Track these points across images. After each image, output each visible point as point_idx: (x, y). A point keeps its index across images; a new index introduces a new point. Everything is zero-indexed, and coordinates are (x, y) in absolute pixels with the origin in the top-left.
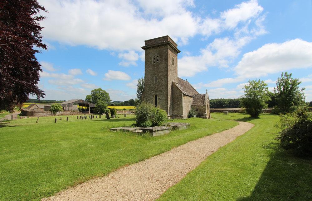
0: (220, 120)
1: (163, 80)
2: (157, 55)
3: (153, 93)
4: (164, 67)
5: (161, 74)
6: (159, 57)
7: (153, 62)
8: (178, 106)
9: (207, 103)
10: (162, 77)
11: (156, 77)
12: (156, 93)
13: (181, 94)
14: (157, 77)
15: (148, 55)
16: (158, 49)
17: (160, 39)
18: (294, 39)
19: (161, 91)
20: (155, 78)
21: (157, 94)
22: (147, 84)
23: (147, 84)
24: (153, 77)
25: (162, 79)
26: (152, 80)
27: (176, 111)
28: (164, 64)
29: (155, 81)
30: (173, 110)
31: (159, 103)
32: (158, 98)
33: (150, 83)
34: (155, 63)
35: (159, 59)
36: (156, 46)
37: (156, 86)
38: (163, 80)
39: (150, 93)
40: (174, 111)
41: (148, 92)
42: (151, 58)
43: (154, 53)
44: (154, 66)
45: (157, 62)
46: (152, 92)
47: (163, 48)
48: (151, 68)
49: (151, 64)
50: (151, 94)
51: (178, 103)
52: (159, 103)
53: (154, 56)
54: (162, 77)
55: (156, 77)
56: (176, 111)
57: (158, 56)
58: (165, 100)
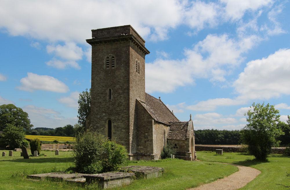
1: (121, 97)
3: (104, 116)
4: (124, 76)
5: (118, 86)
7: (105, 66)
8: (145, 140)
10: (121, 91)
11: (110, 90)
14: (112, 91)
15: (97, 54)
17: (118, 30)
19: (118, 114)
20: (108, 92)
21: (112, 118)
22: (95, 101)
23: (95, 101)
26: (104, 95)
27: (142, 147)
28: (123, 70)
29: (108, 98)
31: (115, 133)
32: (112, 125)
33: (100, 100)
34: (108, 67)
35: (115, 61)
38: (121, 97)
40: (139, 147)
41: (97, 114)
43: (106, 50)
46: (104, 114)
51: (146, 134)
52: (115, 133)
53: (107, 56)
54: (121, 91)
56: (142, 147)
57: (113, 57)
58: (125, 129)
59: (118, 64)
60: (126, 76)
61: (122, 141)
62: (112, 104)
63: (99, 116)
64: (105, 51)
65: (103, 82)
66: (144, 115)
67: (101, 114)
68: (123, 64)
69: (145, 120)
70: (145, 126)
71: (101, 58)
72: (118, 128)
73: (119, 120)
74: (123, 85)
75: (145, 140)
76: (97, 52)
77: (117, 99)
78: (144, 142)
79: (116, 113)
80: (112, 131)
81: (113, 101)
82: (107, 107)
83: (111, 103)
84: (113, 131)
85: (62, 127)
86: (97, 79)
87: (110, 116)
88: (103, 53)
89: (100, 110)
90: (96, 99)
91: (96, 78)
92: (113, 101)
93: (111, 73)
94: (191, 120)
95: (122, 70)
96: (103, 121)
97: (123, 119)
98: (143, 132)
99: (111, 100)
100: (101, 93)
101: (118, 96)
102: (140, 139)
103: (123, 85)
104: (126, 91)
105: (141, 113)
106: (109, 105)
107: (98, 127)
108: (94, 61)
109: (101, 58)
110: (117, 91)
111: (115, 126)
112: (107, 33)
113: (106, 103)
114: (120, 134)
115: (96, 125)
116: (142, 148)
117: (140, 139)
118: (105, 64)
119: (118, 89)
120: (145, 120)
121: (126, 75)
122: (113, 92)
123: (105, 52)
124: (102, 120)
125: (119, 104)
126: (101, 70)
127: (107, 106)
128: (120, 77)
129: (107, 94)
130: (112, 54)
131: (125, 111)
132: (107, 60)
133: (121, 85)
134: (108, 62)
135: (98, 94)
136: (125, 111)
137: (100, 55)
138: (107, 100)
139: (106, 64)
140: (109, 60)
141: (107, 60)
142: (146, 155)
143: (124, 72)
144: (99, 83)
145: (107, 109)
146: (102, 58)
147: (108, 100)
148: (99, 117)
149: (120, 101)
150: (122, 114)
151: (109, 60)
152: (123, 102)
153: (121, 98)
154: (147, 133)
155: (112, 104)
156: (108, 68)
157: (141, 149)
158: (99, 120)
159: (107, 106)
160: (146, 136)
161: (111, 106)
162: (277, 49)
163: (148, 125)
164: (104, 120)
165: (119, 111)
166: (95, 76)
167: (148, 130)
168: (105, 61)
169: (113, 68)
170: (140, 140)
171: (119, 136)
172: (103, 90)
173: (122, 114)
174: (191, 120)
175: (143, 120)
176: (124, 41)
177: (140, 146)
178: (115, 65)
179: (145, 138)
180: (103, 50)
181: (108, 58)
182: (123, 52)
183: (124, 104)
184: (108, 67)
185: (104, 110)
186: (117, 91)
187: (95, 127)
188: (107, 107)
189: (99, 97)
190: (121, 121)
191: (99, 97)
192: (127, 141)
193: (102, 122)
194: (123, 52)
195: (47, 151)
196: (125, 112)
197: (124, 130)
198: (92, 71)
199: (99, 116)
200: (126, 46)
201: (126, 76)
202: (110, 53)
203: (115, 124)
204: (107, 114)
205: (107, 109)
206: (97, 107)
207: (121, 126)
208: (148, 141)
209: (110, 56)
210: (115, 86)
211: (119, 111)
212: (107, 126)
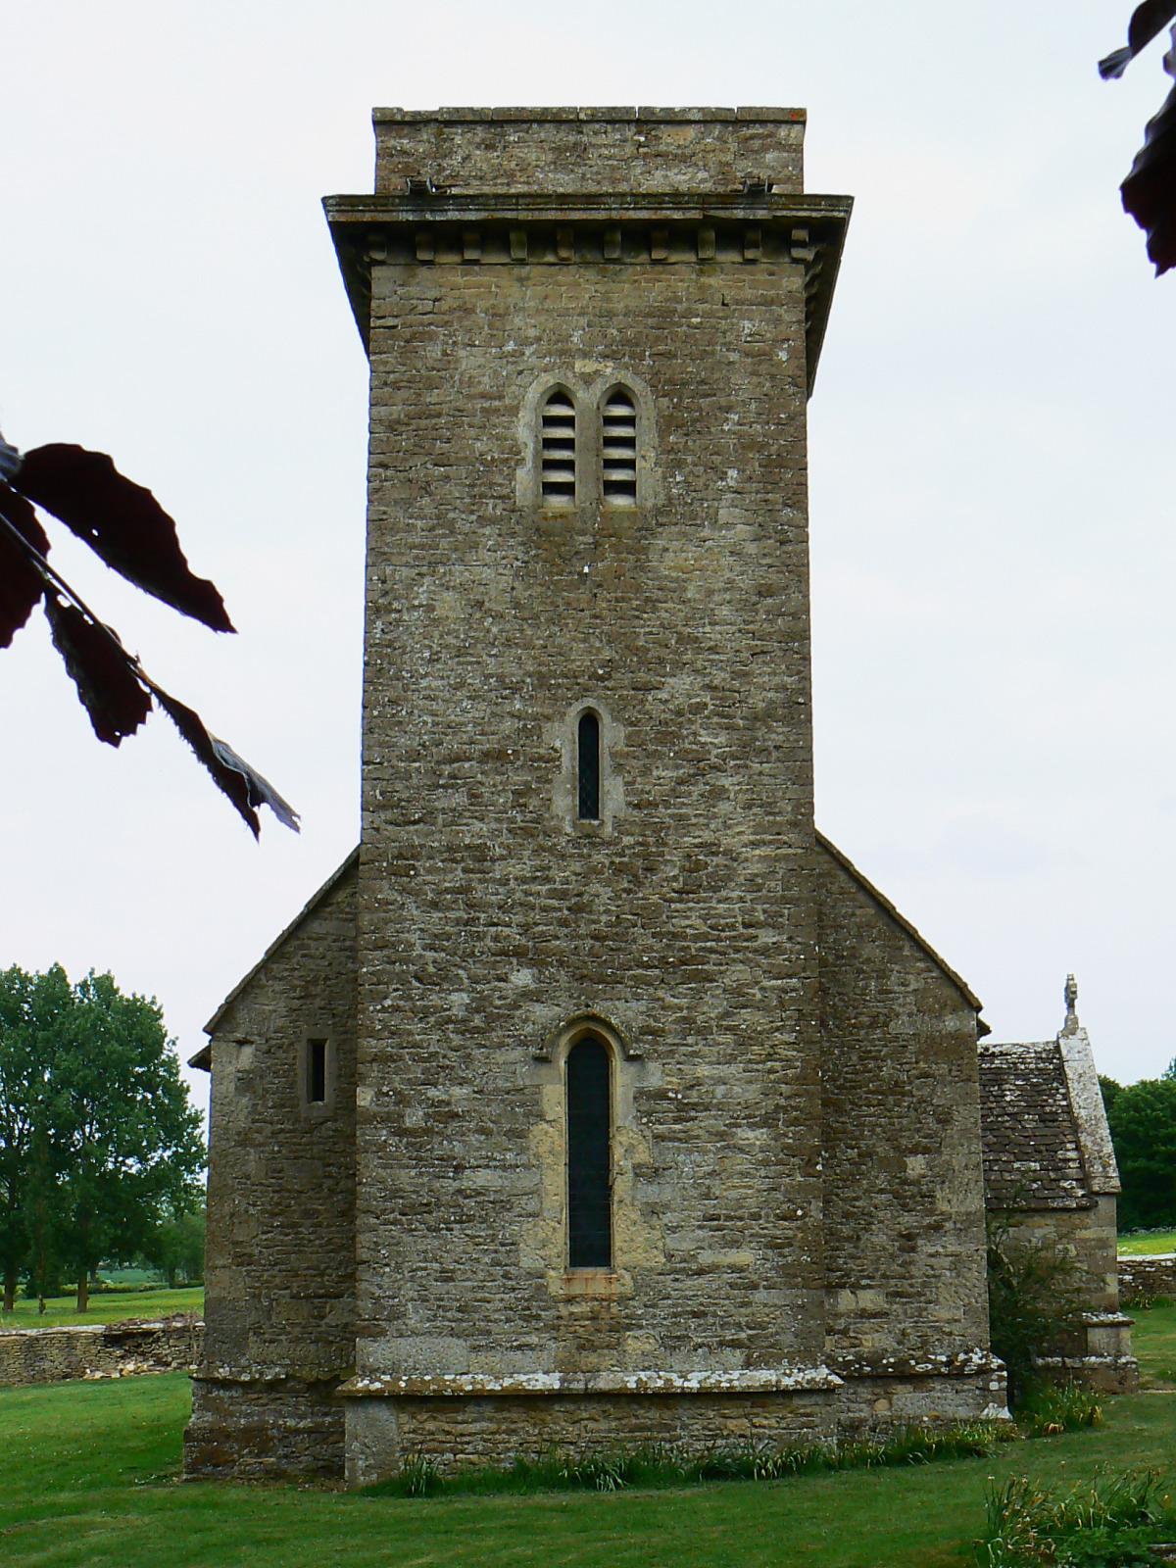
0: (485, 1162)
1: (718, 794)
2: (611, 373)
3: (527, 995)
4: (745, 582)
5: (680, 687)
6: (647, 408)
7: (525, 479)
8: (908, 1220)
9: (1088, 1105)
10: (715, 741)
11: (589, 724)
12: (598, 1009)
13: (950, 1023)
14: (612, 735)
15: (434, 351)
16: (638, 288)
17: (671, 139)
18: (177, 723)
19: (685, 966)
20: (563, 738)
21: (623, 1011)
22: (411, 835)
23: (411, 835)
24: (532, 728)
25: (699, 764)
26: (518, 778)
27: (869, 1299)
28: (734, 524)
29: (564, 802)
30: (832, 1289)
31: (648, 1173)
32: (623, 1081)
33: (474, 831)
34: (567, 489)
35: (646, 433)
36: (612, 224)
37: (591, 873)
38: (718, 794)
39: (479, 1006)
40: (846, 1300)
41: (442, 979)
42: (498, 408)
43: (536, 335)
44: (548, 542)
45: (614, 488)
46: (523, 978)
47: (714, 281)
48: (492, 568)
49: (491, 508)
50: (489, 1020)
51: (916, 1165)
52: (648, 1173)
53: (549, 380)
54: (715, 741)
55: (589, 724)
56: (869, 1299)
57: (620, 395)
58: (767, 1121)
59: (679, 464)
60: (765, 591)
61: (735, 1244)
62: (619, 870)
63: (459, 999)
64: (532, 333)
65: (509, 643)
66: (882, 975)
67: (481, 972)
68: (733, 473)
69: (900, 1026)
70: (897, 1088)
71: (484, 396)
72: (684, 1112)
73: (703, 1032)
74: (735, 675)
75: (908, 1220)
76: (431, 337)
77: (681, 818)
78: (893, 1247)
79: (663, 960)
80: (618, 1153)
81: (627, 840)
82: (563, 895)
83: (600, 857)
84: (630, 1150)
85: (1149, 1078)
86: (430, 608)
87: (595, 996)
88: (510, 347)
89: (480, 937)
90: (428, 818)
91: (423, 599)
92: (627, 840)
93: (597, 545)
94: (1071, 1027)
95: (728, 526)
96: (517, 1054)
97: (746, 1018)
98: (883, 1149)
99: (608, 830)
100: (486, 756)
101: (681, 782)
102: (847, 1215)
103: (735, 675)
104: (778, 734)
105: (854, 956)
106: (585, 877)
107: (455, 1116)
108: (393, 426)
109: (484, 396)
110: (666, 737)
111: (661, 1095)
112: (550, 157)
113: (546, 858)
114: (712, 1174)
115: (432, 1092)
116: (870, 1306)
117: (847, 1215)
118: (528, 454)
119: (679, 713)
120: (900, 1026)
121: (773, 578)
122: (621, 747)
123: (525, 342)
124: (501, 1045)
125: (693, 867)
126: (483, 521)
127: (553, 894)
128: (710, 593)
129: (552, 759)
130: (608, 368)
131: (767, 937)
132: (550, 421)
133: (719, 677)
134: (568, 444)
135: (447, 769)
136: (767, 937)
137: (468, 361)
138: (558, 831)
139: (536, 454)
140: (568, 422)
141: (550, 421)
142: (926, 1376)
143: (752, 548)
144: (460, 652)
145: (563, 923)
146: (501, 397)
147: (568, 829)
148: (458, 1012)
149: (707, 836)
150: (738, 973)
151: (568, 422)
152: (747, 852)
153: (723, 807)
154: (926, 1151)
155: (619, 870)
156: (558, 502)
157: (863, 1314)
158: (457, 1040)
159: (553, 894)
160: (910, 1190)
161: (601, 893)
162: (74, 678)
163: (926, 1075)
164: (523, 1044)
165: (696, 938)
166: (406, 572)
167: (931, 1123)
168: (525, 431)
169: (620, 501)
170: (846, 1231)
171: (707, 1196)
172: (508, 726)
173: (738, 973)
174: (1071, 1027)
175: (873, 1025)
176: (750, 254)
177: (855, 1288)
178: (647, 472)
179: (905, 1208)
180: (497, 315)
181: (560, 396)
182: (733, 357)
183: (755, 868)
184: (567, 489)
185: (525, 928)
186: (666, 737)
187: (414, 1118)
188: (563, 895)
189: (459, 799)
190: (729, 1038)
191: (459, 799)
192: (789, 1243)
193: (500, 1057)
194: (733, 357)
195: (899, 1459)
196: (764, 951)
197: (754, 1137)
198: (377, 525)
199: (459, 999)
200: (767, 302)
201: (765, 591)
202: (585, 355)
203: (655, 1077)
204: (563, 976)
205: (563, 923)
206: (434, 905)
207: (720, 1090)
208: (937, 1227)
209: (587, 380)
210: (647, 688)
211: (696, 938)
212: (554, 1097)
